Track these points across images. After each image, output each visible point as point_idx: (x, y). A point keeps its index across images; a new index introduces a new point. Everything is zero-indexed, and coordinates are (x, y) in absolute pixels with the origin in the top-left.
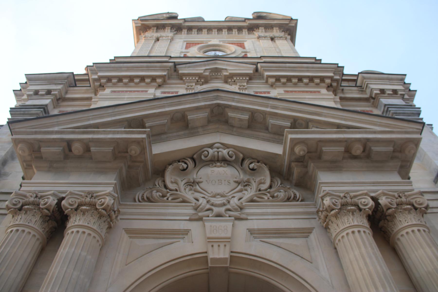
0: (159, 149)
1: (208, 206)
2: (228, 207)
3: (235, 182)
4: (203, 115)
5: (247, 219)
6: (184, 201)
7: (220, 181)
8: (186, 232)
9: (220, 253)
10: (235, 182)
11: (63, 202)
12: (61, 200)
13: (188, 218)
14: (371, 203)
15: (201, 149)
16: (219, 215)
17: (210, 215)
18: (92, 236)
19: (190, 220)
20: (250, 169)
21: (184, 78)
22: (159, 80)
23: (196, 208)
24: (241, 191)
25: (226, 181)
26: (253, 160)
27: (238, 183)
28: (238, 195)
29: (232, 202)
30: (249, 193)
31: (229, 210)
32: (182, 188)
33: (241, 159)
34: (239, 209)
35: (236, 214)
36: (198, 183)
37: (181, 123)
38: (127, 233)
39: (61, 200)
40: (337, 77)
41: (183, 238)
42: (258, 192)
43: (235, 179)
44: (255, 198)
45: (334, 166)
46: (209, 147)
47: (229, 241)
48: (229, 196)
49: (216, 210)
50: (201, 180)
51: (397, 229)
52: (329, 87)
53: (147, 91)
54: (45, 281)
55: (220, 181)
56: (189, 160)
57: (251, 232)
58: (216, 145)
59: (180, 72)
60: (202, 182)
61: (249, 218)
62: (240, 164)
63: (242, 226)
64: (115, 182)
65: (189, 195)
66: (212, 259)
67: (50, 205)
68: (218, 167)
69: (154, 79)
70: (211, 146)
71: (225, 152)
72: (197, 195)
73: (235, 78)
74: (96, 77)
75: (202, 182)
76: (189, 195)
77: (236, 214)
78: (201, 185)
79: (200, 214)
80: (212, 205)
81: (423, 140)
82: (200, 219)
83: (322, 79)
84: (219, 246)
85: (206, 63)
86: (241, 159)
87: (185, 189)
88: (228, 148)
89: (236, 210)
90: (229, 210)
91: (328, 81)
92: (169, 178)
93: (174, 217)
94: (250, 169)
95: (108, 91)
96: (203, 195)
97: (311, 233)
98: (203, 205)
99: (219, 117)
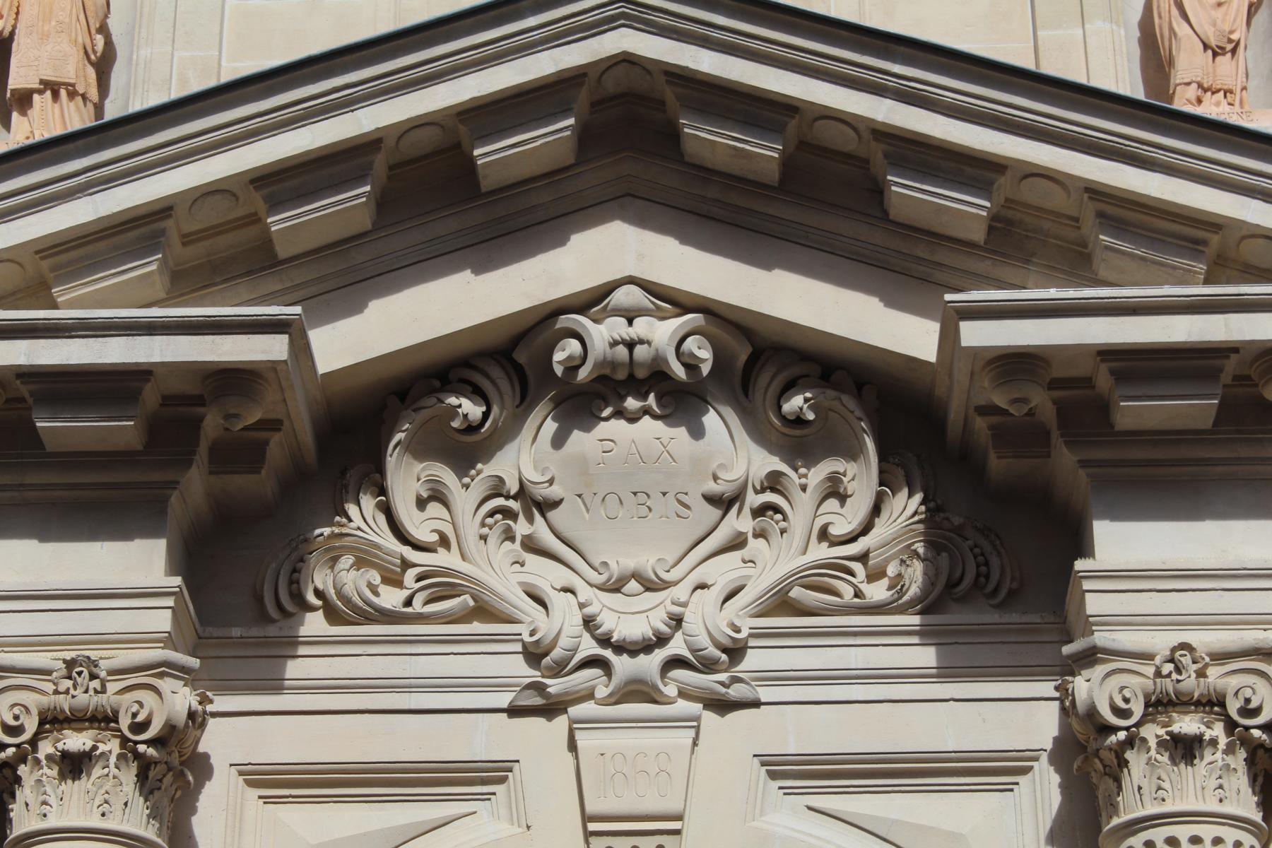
1: (589, 647)
2: (677, 647)
3: (712, 499)
4: (552, 135)
5: (756, 704)
7: (642, 498)
10: (712, 499)
15: (542, 324)
16: (639, 691)
17: (602, 692)
18: (1208, 842)
19: (514, 711)
20: (783, 418)
23: (534, 655)
24: (737, 543)
25: (670, 496)
27: (724, 503)
28: (725, 570)
29: (693, 622)
30: (776, 561)
31: (676, 662)
32: (470, 527)
33: (754, 366)
34: (724, 657)
35: (708, 681)
42: (822, 552)
43: (712, 487)
44: (797, 592)
46: (582, 309)
47: (677, 832)
48: (676, 583)
49: (623, 665)
50: (555, 491)
55: (642, 498)
57: (786, 770)
58: (627, 296)
60: (556, 504)
61: (765, 694)
65: (497, 569)
68: (633, 419)
70: (592, 301)
71: (660, 333)
72: (544, 574)
75: (556, 504)
78: (552, 515)
79: (556, 686)
80: (605, 641)
82: (551, 709)
86: (754, 366)
87: (484, 538)
88: (685, 309)
89: (708, 666)
98: (564, 642)
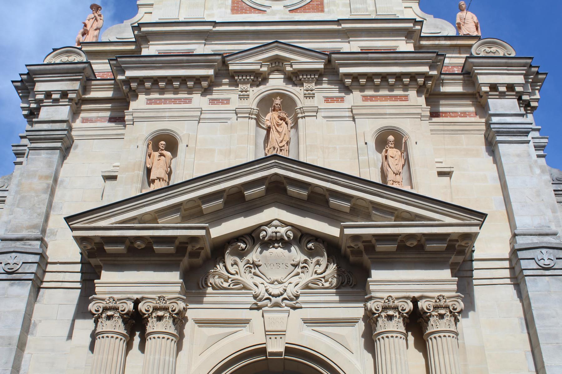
1: (267, 296)
2: (285, 296)
3: (292, 265)
5: (301, 308)
9: (276, 346)
10: (292, 265)
11: (140, 306)
12: (137, 302)
13: (249, 306)
14: (411, 305)
15: (258, 228)
17: (269, 305)
19: (251, 309)
20: (307, 248)
22: (205, 84)
27: (295, 266)
28: (295, 280)
30: (306, 278)
32: (242, 270)
38: (196, 323)
39: (137, 302)
40: (435, 73)
44: (310, 285)
45: (388, 262)
46: (266, 225)
47: (285, 335)
49: (273, 299)
51: (427, 332)
53: (189, 101)
56: (248, 238)
60: (260, 266)
61: (303, 306)
62: (298, 240)
64: (182, 280)
65: (248, 279)
66: (269, 353)
67: (129, 311)
69: (198, 80)
72: (258, 280)
73: (301, 77)
74: (123, 77)
75: (260, 266)
79: (260, 304)
80: (270, 294)
81: (479, 237)
82: (259, 308)
83: (413, 77)
84: (276, 338)
85: (263, 48)
89: (291, 300)
91: (421, 80)
92: (229, 259)
93: (236, 305)
94: (307, 248)
95: (142, 97)
97: (357, 322)
98: (261, 294)
99: (277, 191)
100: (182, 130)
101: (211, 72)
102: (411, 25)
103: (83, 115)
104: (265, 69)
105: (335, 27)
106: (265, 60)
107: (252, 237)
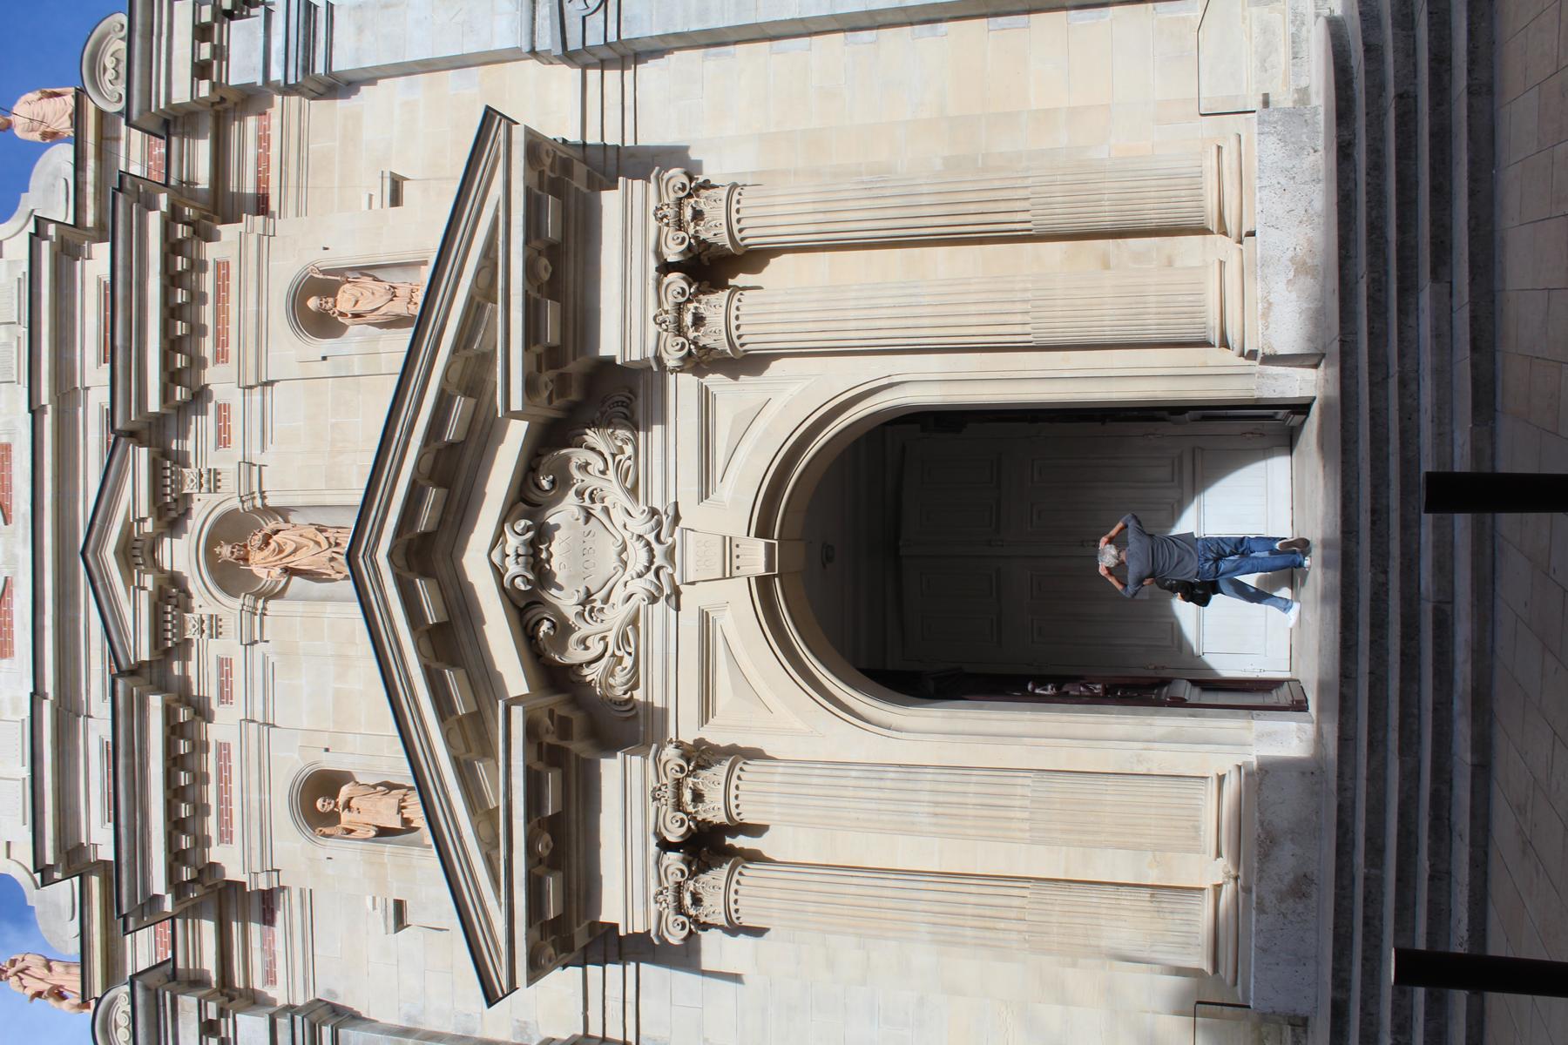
0: (515, 681)
1: (651, 576)
2: (651, 537)
3: (587, 522)
6: (634, 622)
8: (705, 619)
9: (755, 557)
10: (587, 522)
13: (673, 613)
15: (508, 595)
16: (670, 554)
17: (670, 570)
19: (678, 608)
21: (1030, 687)
23: (653, 599)
26: (530, 482)
27: (589, 516)
28: (618, 516)
30: (614, 494)
31: (658, 537)
35: (666, 523)
36: (589, 594)
37: (450, 641)
41: (714, 621)
42: (611, 473)
44: (628, 485)
49: (658, 561)
52: (204, 233)
54: (574, 838)
56: (529, 615)
57: (704, 494)
59: (145, 655)
61: (672, 500)
63: (691, 514)
65: (615, 616)
69: (174, 731)
70: (498, 572)
71: (513, 542)
72: (618, 595)
73: (169, 499)
76: (615, 616)
77: (666, 523)
79: (667, 591)
80: (648, 569)
82: (677, 592)
83: (172, 248)
89: (659, 524)
90: (658, 537)
91: (181, 231)
92: (574, 655)
96: (620, 585)
99: (427, 553)
100: (291, 763)
101: (156, 702)
102: (45, 245)
103: (257, 983)
104: (149, 581)
105: (48, 420)
106: (128, 580)
107: (526, 608)
